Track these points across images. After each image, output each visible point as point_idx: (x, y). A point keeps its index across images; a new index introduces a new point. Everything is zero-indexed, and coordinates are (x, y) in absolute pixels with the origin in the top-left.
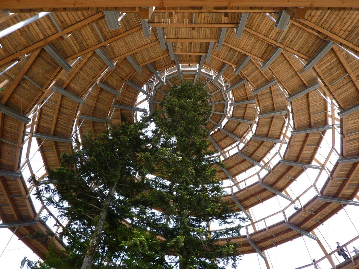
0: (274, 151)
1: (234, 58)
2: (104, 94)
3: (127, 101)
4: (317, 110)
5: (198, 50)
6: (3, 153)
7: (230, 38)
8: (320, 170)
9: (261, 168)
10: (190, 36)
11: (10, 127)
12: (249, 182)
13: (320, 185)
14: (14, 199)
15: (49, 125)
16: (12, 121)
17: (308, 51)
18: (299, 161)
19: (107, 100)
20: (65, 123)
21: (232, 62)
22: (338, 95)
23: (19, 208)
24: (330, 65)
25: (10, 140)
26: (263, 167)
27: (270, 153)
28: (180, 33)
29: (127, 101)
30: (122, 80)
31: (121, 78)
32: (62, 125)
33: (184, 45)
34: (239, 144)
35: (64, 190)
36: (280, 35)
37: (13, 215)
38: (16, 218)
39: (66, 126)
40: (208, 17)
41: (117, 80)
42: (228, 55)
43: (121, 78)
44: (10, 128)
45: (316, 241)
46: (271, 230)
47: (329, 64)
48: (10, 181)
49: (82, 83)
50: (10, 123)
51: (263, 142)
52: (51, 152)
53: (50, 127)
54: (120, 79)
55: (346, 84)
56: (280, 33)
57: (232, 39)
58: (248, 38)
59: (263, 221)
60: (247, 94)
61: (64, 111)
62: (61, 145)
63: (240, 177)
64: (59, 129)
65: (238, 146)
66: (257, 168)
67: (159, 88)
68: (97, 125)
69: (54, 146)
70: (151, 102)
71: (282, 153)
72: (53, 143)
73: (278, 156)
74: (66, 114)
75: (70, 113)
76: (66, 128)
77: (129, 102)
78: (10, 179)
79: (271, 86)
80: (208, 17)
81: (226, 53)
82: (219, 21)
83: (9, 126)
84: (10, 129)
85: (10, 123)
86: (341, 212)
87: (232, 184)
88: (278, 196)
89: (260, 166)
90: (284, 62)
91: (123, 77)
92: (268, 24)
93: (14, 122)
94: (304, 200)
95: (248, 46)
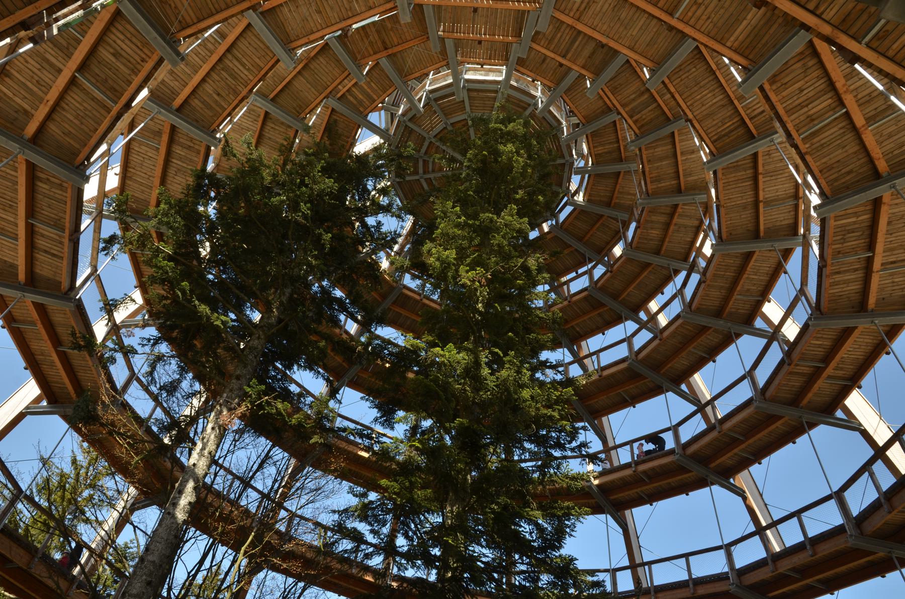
0: (616, 333)
1: (643, 112)
2: (324, 62)
3: (356, 98)
4: (748, 290)
5: (581, 61)
6: (64, 109)
7: (681, 73)
8: (881, 444)
9: (637, 326)
10: (605, 28)
11: (116, 55)
12: (607, 358)
13: (763, 375)
14: (37, 229)
15: (177, 83)
16: (127, 41)
17: (836, 180)
18: (762, 234)
19: (325, 80)
20: (218, 94)
21: (634, 118)
22: (832, 285)
23: (38, 255)
24: (855, 223)
25: (98, 84)
26: (643, 326)
27: (663, 294)
28: (591, 12)
29: (356, 98)
30: (382, 48)
31: (384, 42)
32: (210, 96)
33: (559, 35)
34: (594, 267)
35: (182, 255)
36: (811, 125)
37: (14, 267)
38: (22, 276)
39: (216, 102)
40: (709, 18)
41: (371, 43)
42: (634, 100)
43: (384, 42)
44: (114, 55)
45: (621, 531)
46: (728, 425)
47: (854, 219)
48: (46, 183)
49: (309, 19)
50: (119, 42)
51: (676, 206)
52: (151, 147)
53: (175, 88)
54: (380, 44)
55: (856, 270)
56: (813, 120)
57: (683, 77)
58: (714, 90)
59: (795, 520)
60: (615, 195)
61: (231, 65)
62: (181, 140)
63: (594, 343)
64: (196, 101)
65: (590, 273)
66: (631, 326)
67: (436, 100)
68: (273, 126)
69: (165, 138)
70: (404, 122)
71: (689, 292)
72: (167, 130)
73: (625, 345)
74: (231, 75)
75: (242, 75)
76: (215, 106)
77: (360, 102)
78: (48, 179)
79: (681, 203)
80: (709, 18)
81: (633, 96)
82: (722, 38)
83: (112, 51)
84: (113, 59)
85: (119, 42)
86: (803, 440)
87: (569, 358)
88: (670, 394)
89: (637, 320)
90: (748, 172)
91: (388, 42)
92: (805, 92)
93: (134, 47)
94: (723, 408)
95: (704, 108)
